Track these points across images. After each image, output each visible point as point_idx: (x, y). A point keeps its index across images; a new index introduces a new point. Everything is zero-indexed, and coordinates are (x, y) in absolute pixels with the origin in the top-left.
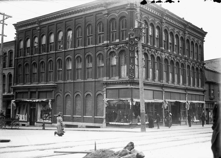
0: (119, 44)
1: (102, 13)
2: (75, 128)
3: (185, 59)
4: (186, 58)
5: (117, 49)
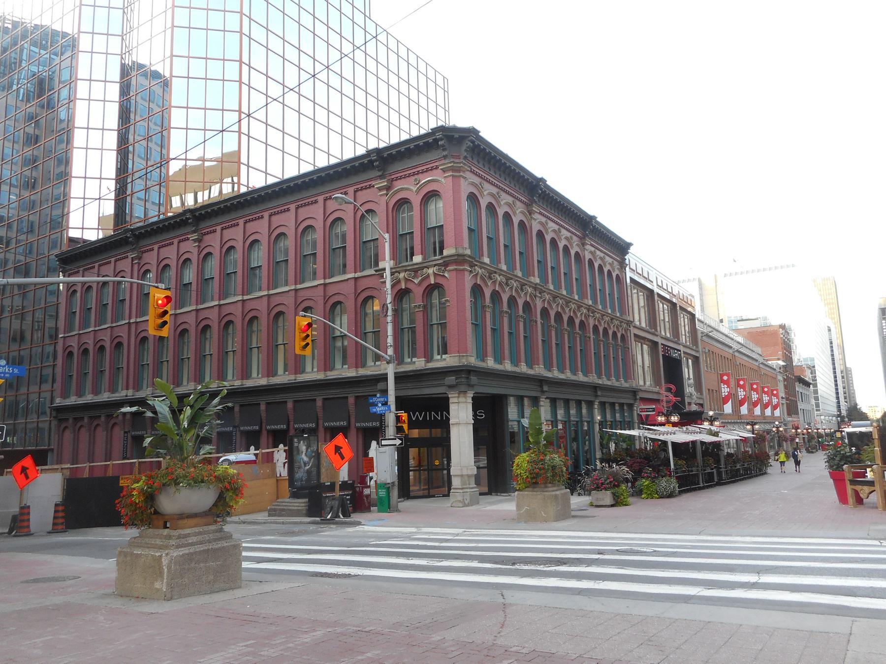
0: (423, 268)
1: (373, 186)
2: (837, 605)
3: (535, 287)
5: (416, 281)
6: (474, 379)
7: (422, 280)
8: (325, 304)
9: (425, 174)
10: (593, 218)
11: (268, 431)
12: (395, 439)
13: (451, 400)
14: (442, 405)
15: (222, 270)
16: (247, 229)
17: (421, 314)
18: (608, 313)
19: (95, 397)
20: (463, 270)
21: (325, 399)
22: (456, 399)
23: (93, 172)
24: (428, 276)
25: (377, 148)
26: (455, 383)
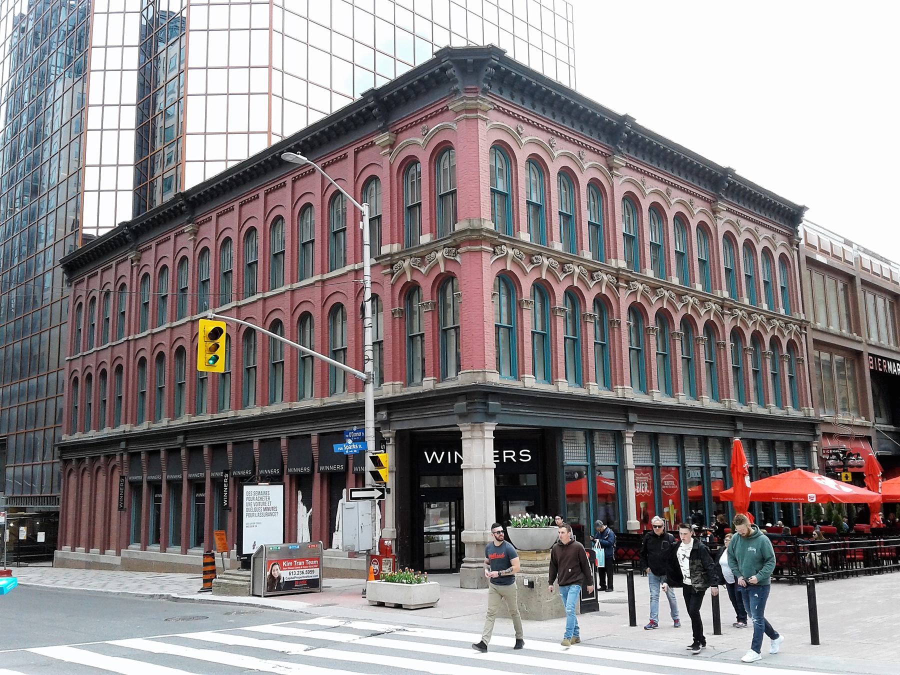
4: (725, 299)
5: (423, 270)
6: (494, 404)
7: (432, 269)
8: (323, 306)
9: (435, 120)
10: (727, 172)
11: (322, 474)
12: (373, 490)
13: (464, 435)
14: (454, 442)
15: (218, 269)
16: (243, 213)
17: (430, 314)
18: (744, 305)
19: (83, 436)
20: (481, 251)
21: (321, 435)
22: (469, 433)
23: (109, 158)
24: (437, 264)
25: (373, 90)
26: (465, 411)
